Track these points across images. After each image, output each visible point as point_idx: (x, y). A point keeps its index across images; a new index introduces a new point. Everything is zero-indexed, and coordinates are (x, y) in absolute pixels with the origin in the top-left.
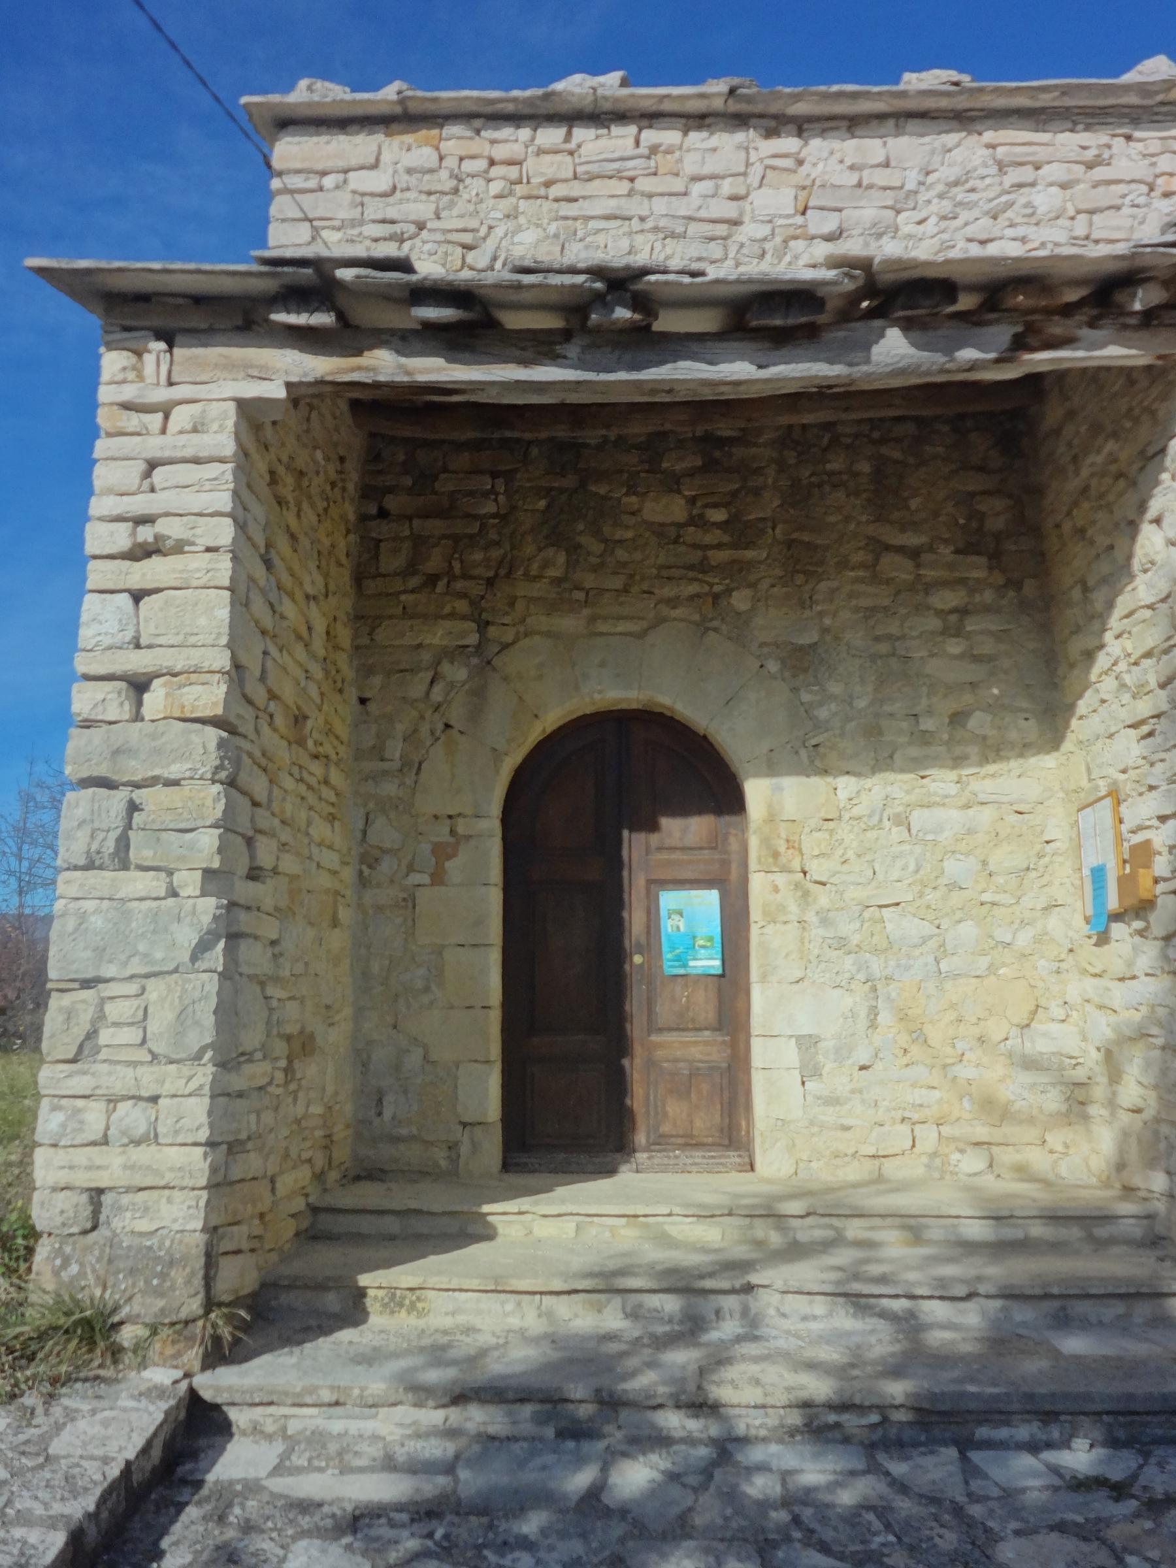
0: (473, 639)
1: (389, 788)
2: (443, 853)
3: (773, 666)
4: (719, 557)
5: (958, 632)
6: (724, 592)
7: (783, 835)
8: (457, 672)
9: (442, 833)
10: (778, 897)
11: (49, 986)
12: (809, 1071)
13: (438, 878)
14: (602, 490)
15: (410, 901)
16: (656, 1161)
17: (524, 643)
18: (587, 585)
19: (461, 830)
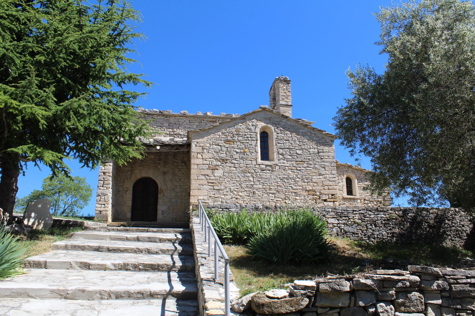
1: (121, 184)
2: (126, 191)
8: (129, 173)
9: (126, 189)
11: (197, 252)
13: (126, 194)
15: (123, 196)
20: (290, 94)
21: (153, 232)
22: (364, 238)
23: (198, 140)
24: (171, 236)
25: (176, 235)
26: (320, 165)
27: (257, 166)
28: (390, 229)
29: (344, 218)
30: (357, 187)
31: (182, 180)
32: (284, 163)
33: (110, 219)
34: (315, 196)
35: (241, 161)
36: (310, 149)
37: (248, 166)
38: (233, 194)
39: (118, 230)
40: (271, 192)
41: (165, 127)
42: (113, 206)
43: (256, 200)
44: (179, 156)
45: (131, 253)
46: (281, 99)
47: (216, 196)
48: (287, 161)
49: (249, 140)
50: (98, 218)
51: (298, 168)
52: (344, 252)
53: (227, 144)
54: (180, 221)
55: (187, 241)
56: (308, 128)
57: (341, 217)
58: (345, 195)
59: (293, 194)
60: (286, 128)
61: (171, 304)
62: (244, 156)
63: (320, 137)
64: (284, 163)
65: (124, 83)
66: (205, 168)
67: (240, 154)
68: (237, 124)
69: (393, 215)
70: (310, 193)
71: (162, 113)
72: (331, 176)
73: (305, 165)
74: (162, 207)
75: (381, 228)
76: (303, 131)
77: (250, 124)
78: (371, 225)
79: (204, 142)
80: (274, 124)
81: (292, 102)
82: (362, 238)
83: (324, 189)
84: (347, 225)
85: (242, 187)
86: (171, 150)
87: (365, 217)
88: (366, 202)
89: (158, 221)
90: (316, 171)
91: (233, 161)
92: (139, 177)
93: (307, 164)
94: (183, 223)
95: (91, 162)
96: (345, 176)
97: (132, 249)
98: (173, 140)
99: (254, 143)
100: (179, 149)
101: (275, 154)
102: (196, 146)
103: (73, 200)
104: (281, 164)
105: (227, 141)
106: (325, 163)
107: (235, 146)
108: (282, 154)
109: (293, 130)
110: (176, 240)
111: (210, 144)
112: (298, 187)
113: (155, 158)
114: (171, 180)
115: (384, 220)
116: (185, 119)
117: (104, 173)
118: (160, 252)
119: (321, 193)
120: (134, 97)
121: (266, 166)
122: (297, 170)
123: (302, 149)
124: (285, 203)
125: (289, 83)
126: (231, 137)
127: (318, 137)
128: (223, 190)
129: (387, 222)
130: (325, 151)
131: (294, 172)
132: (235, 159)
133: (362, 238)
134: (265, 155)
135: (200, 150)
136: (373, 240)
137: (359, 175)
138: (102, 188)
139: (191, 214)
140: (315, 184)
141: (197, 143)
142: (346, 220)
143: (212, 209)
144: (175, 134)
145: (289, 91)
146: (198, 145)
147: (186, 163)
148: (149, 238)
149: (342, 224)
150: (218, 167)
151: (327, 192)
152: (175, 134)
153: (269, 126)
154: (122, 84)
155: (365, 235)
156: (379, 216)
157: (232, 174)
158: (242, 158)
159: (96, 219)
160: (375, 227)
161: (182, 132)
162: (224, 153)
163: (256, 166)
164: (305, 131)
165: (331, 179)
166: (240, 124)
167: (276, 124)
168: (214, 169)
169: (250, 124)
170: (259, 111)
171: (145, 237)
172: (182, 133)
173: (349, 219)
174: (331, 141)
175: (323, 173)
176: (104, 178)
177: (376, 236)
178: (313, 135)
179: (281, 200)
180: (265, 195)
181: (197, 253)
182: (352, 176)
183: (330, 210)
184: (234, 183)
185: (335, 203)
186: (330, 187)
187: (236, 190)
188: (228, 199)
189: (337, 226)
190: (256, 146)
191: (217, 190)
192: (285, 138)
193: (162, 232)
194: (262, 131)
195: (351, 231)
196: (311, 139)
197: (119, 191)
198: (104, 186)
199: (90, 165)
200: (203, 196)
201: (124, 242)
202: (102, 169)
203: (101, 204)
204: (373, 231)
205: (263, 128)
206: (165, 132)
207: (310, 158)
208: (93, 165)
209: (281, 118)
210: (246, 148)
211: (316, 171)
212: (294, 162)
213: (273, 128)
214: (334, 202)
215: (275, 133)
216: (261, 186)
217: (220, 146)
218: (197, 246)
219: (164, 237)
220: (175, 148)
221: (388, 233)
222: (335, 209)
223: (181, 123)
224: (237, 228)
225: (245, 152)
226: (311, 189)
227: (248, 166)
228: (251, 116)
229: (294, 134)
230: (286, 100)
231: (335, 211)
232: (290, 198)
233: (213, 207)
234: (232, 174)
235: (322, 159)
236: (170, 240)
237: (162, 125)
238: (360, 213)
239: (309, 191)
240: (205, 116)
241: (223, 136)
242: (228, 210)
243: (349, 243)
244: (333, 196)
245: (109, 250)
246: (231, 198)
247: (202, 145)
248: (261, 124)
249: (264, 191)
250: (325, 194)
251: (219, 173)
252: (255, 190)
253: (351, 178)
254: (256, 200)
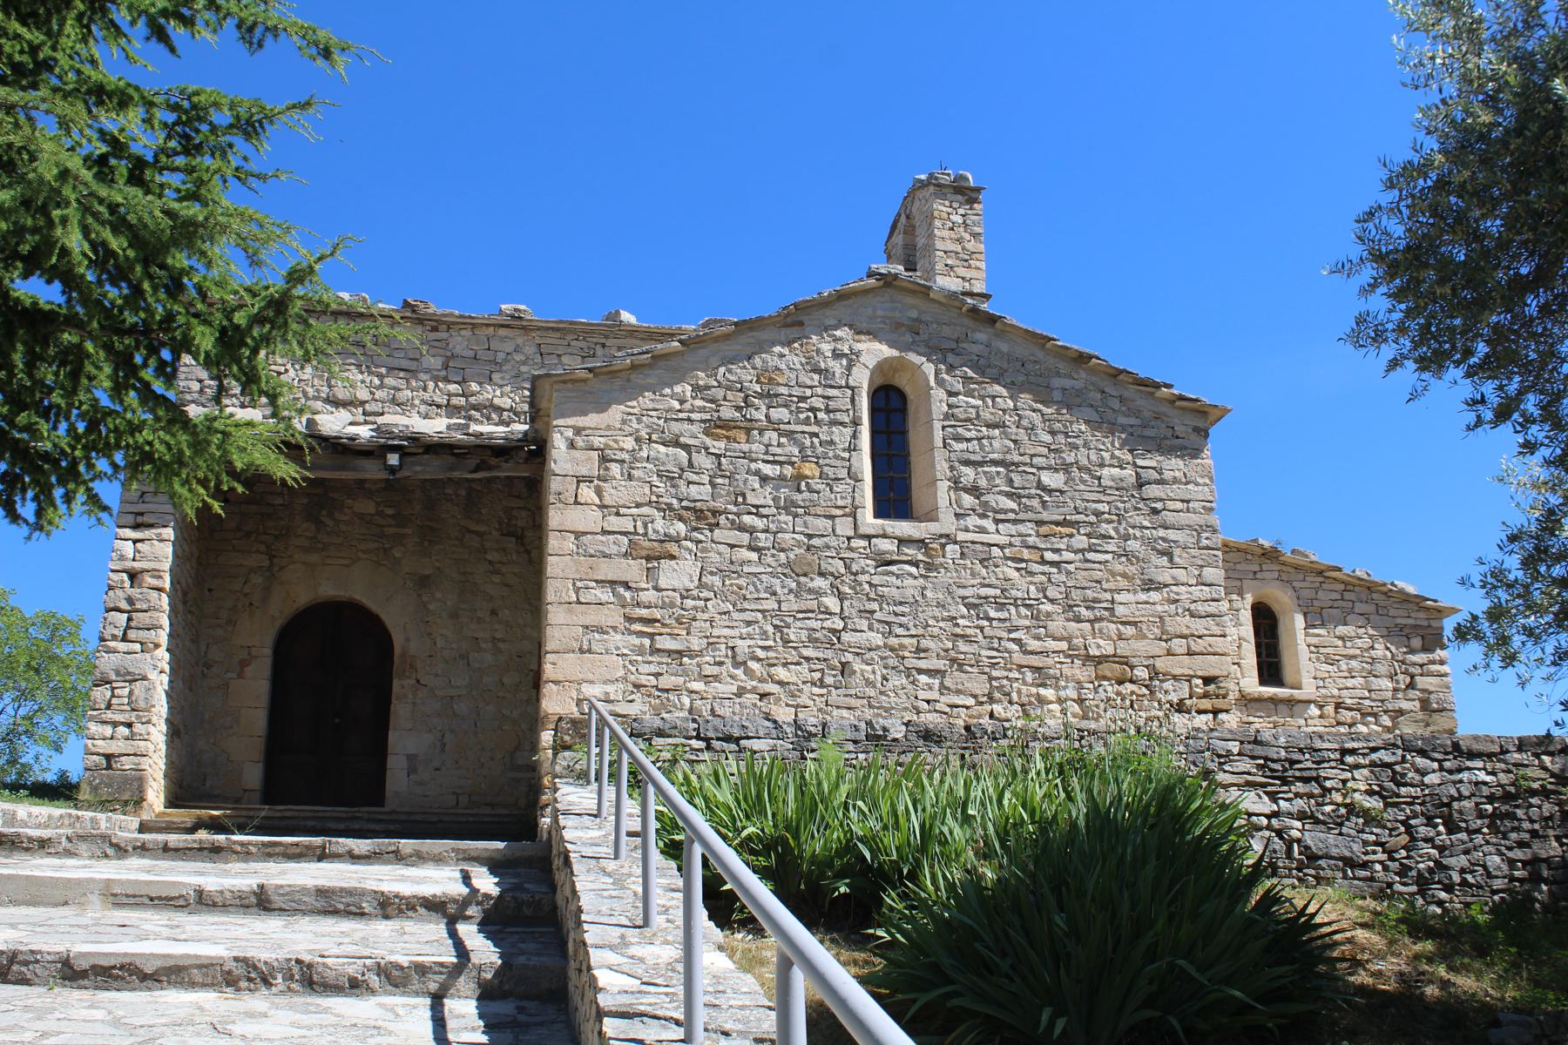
0: (267, 563)
1: (220, 632)
2: (244, 664)
4: (392, 530)
5: (497, 572)
8: (257, 580)
12: (412, 770)
13: (240, 676)
14: (336, 496)
20: (982, 247)
21: (354, 857)
22: (1398, 887)
23: (580, 421)
24: (441, 880)
25: (466, 878)
26: (1150, 543)
27: (856, 543)
28: (1521, 844)
29: (1299, 787)
30: (1302, 647)
31: (505, 614)
32: (982, 530)
33: (156, 795)
34: (1130, 687)
35: (783, 518)
36: (1102, 465)
37: (816, 542)
38: (749, 673)
39: (166, 849)
40: (923, 664)
41: (428, 371)
42: (175, 732)
43: (853, 702)
44: (488, 503)
45: (204, 985)
46: (939, 267)
47: (666, 682)
48: (997, 522)
49: (818, 422)
50: (95, 789)
51: (1049, 556)
52: (1356, 964)
53: (717, 438)
54: (491, 805)
55: (527, 911)
56: (1093, 371)
57: (1285, 782)
58: (1251, 683)
59: (1029, 676)
60: (989, 369)
61: (464, 1010)
62: (798, 497)
63: (1146, 414)
64: (982, 530)
65: (188, 22)
66: (614, 549)
67: (777, 489)
68: (763, 348)
69: (1529, 772)
70: (1106, 669)
71: (413, 309)
72: (1198, 592)
73: (1081, 541)
74: (406, 740)
75: (1479, 839)
76: (1067, 383)
77: (826, 348)
78: (1430, 822)
79: (609, 428)
80: (937, 351)
81: (987, 281)
82: (1390, 885)
83: (1169, 653)
84: (1317, 822)
85: (786, 642)
86: (451, 469)
87: (1399, 784)
88: (1347, 716)
89: (391, 803)
90: (1132, 569)
91: (747, 519)
92: (303, 597)
93: (1088, 535)
94: (504, 812)
95: (30, 494)
96: (1249, 599)
97: (207, 966)
98: (458, 427)
99: (842, 436)
100: (490, 468)
101: (943, 486)
102: (572, 445)
103: (22, 712)
104: (970, 536)
105: (716, 427)
106: (1171, 534)
107: (754, 447)
108: (974, 490)
109: (1021, 378)
110: (465, 903)
111: (638, 440)
112: (1051, 645)
113: (380, 514)
114: (454, 616)
115: (1491, 799)
116: (520, 341)
117: (133, 576)
118: (374, 980)
119: (1155, 674)
120: (250, 127)
121: (903, 541)
122: (1043, 562)
123: (1066, 468)
124: (992, 716)
125: (975, 201)
126: (738, 409)
127: (1137, 413)
128: (700, 653)
129: (1503, 809)
130: (1168, 475)
131: (1031, 574)
132: (757, 511)
133: (1390, 885)
134: (895, 495)
135: (588, 464)
136: (1443, 895)
137: (1311, 594)
138: (122, 646)
139: (546, 766)
140: (1129, 631)
141: (578, 431)
142: (1310, 796)
143: (657, 741)
144: (476, 408)
145: (975, 235)
146: (580, 442)
147: (520, 539)
148: (321, 892)
149: (1290, 815)
150: (673, 548)
151: (1181, 666)
152: (476, 408)
153: (914, 358)
154: (175, 30)
155: (1403, 871)
156: (1465, 776)
157: (742, 582)
158: (789, 507)
159: (84, 795)
160: (1450, 832)
161: (506, 397)
162: (705, 479)
163: (854, 543)
164: (1078, 385)
165: (1202, 608)
166: (777, 349)
167: (943, 352)
168: (656, 555)
169: (826, 348)
170: (866, 292)
171: (304, 890)
172: (506, 402)
173: (1326, 791)
174: (1196, 430)
175: (1165, 577)
176: (130, 600)
177: (1456, 878)
178: (1116, 405)
179: (971, 702)
180: (898, 681)
181: (601, 1014)
182: (1281, 598)
183: (1235, 747)
184: (749, 623)
185: (1222, 716)
186: (1198, 645)
187: (761, 654)
188: (722, 695)
189: (1269, 827)
190: (852, 448)
191: (669, 652)
192: (986, 415)
193: (398, 857)
194: (879, 381)
195: (1334, 852)
196: (1104, 423)
197: (208, 666)
198: (132, 634)
199: (27, 510)
200: (605, 683)
201: (180, 917)
202: (122, 558)
203: (115, 724)
204: (1441, 849)
205: (882, 367)
206: (427, 396)
207: (1100, 507)
208: (39, 513)
209: (967, 322)
210: (804, 459)
211: (1132, 569)
212: (1028, 528)
213: (929, 369)
214: (1216, 712)
215: (939, 394)
216: (878, 639)
217: (686, 448)
218: (596, 956)
219: (406, 890)
220: (473, 462)
221: (1511, 863)
222: (1256, 742)
223: (501, 357)
224: (796, 837)
225: (799, 477)
226: (1110, 650)
227: (816, 542)
228: (828, 312)
229: (1026, 399)
230: (961, 271)
231: (1259, 750)
232: (1015, 696)
233: (661, 733)
234: (742, 582)
235: (1155, 511)
236: (435, 906)
237: (413, 365)
238: (1373, 764)
239: (1099, 660)
240: (614, 328)
241: (699, 403)
242: (733, 747)
243: (1367, 917)
244: (1212, 687)
245: (71, 973)
246: (739, 695)
247: (598, 441)
248: (875, 351)
249: (891, 662)
250: (1175, 678)
251: (678, 574)
252: (849, 657)
253: (1276, 608)
254: (853, 702)
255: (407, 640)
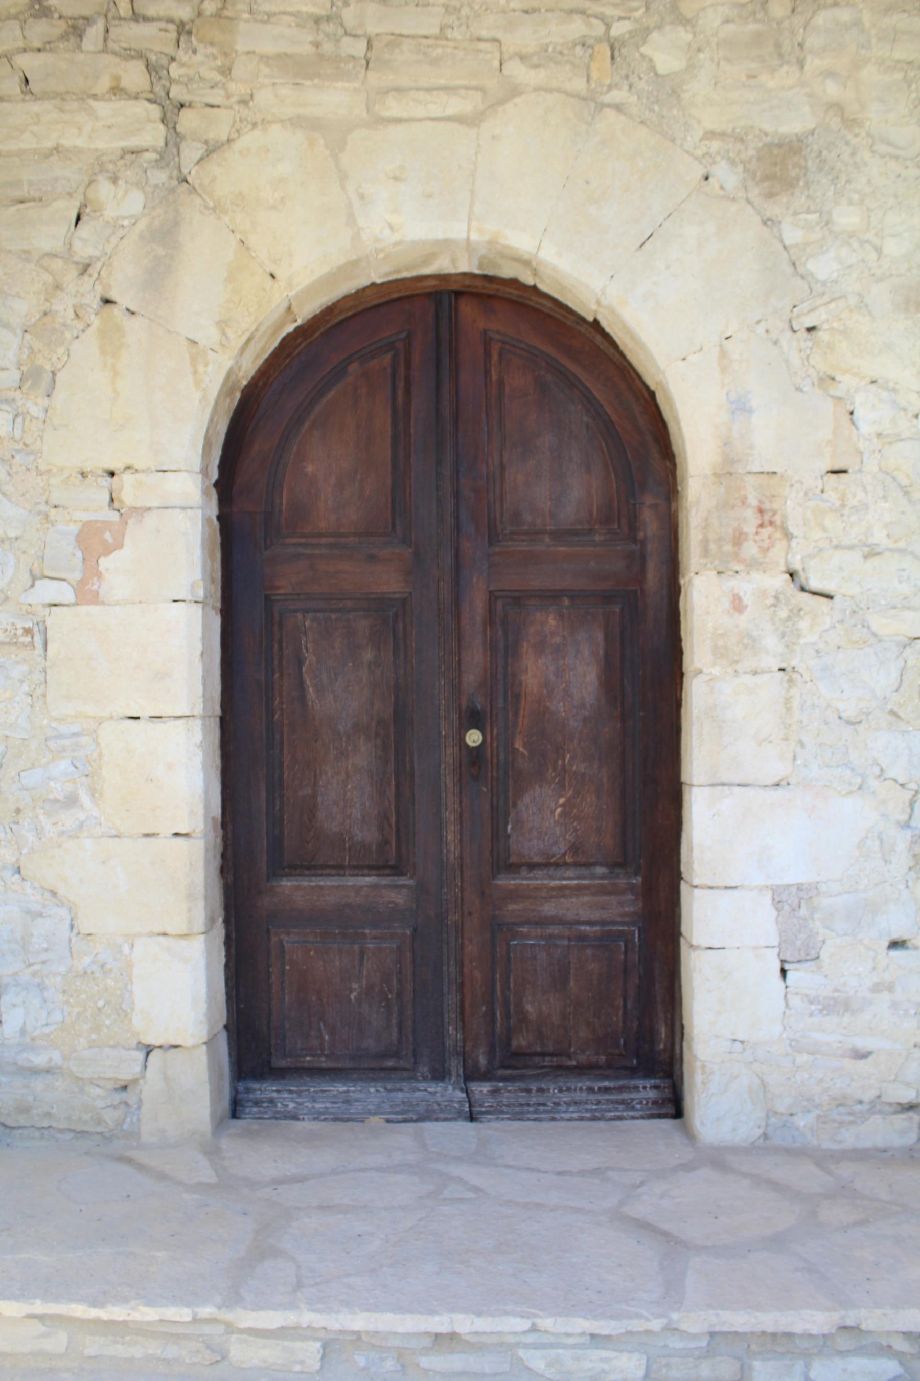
0: (153, 135)
2: (95, 543)
3: (727, 176)
6: (632, 34)
7: (753, 501)
8: (123, 202)
9: (92, 503)
10: (743, 620)
13: (87, 593)
15: (35, 635)
16: (505, 1098)
17: (250, 139)
18: (372, 29)
19: (128, 496)
255: (740, 407)
